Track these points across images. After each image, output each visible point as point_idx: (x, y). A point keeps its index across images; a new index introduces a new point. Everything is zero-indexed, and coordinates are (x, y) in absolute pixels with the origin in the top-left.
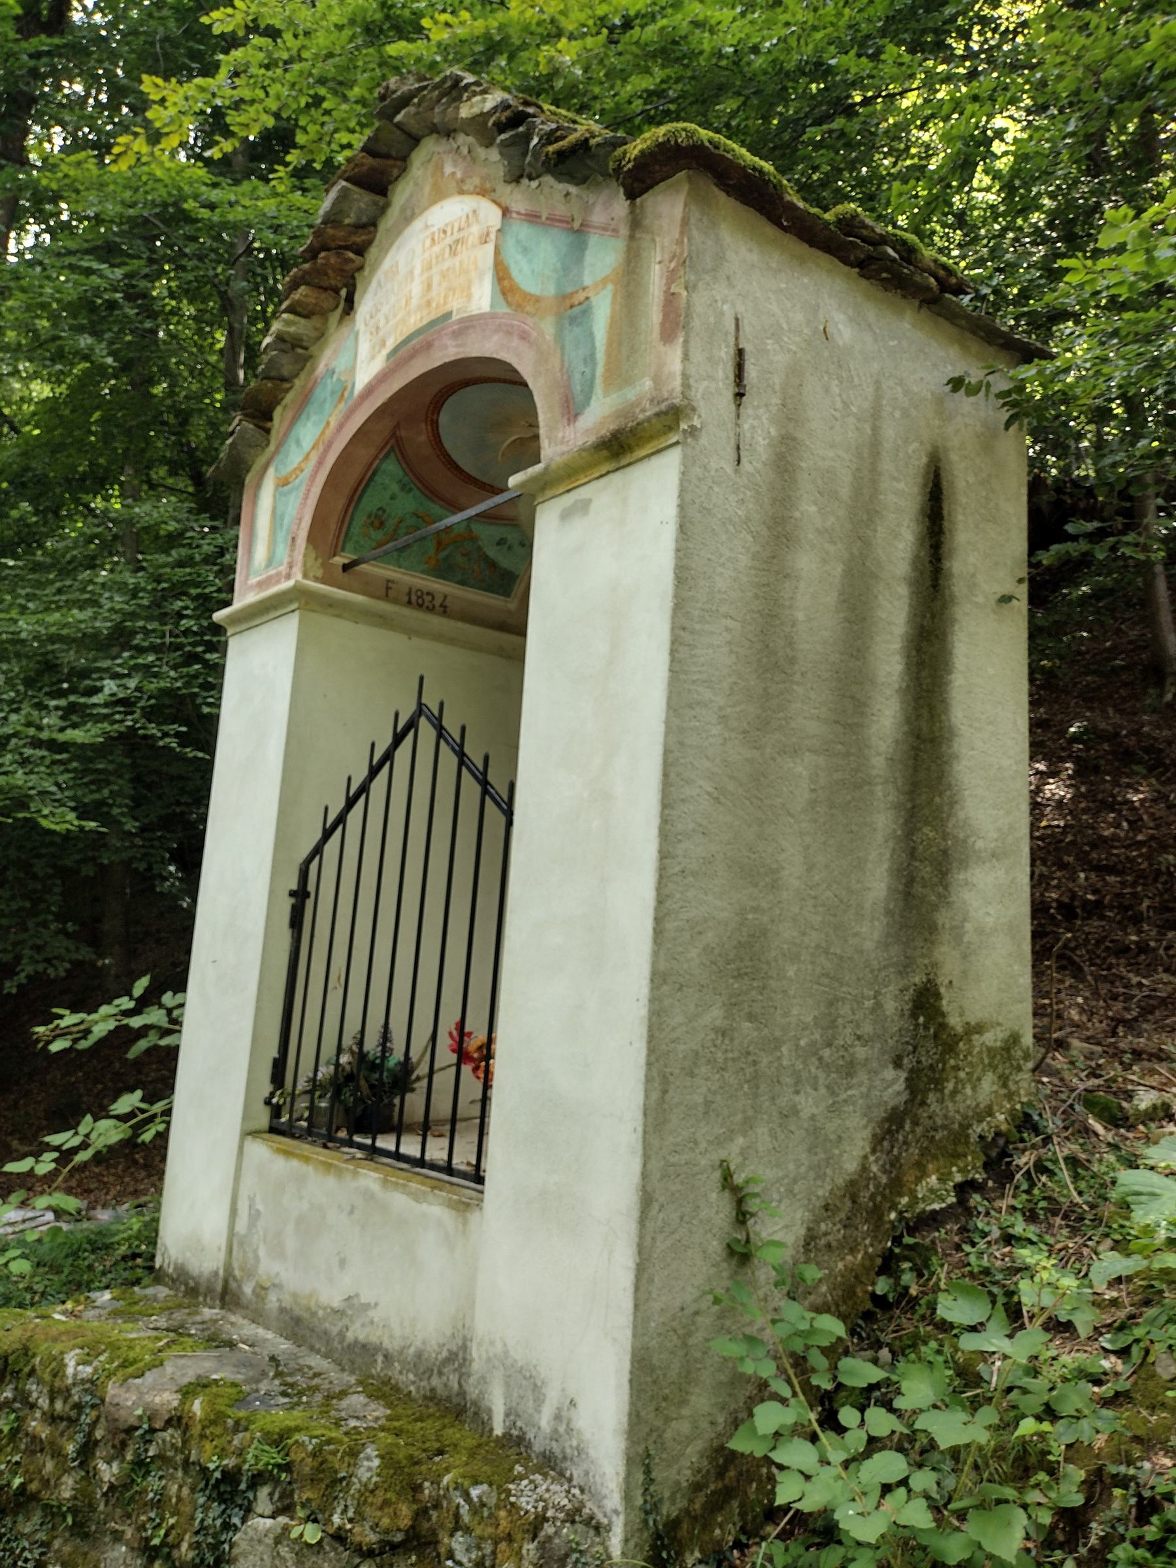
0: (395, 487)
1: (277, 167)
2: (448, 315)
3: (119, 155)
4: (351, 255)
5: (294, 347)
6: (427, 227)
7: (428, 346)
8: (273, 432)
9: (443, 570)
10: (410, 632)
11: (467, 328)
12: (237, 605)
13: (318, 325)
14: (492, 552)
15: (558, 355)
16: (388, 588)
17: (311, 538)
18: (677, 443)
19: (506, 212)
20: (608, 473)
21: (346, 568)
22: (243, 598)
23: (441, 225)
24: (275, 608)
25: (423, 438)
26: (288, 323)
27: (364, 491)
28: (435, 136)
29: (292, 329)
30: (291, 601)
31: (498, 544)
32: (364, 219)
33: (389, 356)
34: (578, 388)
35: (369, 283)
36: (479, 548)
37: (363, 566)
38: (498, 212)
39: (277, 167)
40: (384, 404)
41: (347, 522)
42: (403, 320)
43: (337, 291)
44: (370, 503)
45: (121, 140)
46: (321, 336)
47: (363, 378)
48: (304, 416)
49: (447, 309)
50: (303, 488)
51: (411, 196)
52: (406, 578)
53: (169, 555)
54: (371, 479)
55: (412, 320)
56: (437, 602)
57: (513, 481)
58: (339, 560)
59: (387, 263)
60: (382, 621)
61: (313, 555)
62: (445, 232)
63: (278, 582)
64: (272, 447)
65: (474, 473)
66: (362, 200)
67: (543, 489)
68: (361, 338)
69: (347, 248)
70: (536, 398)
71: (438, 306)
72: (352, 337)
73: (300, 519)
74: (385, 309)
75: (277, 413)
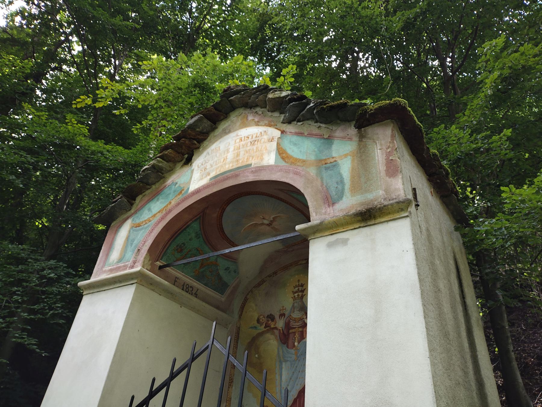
0: (193, 235)
1: (138, 124)
2: (251, 165)
3: (79, 102)
4: (195, 142)
5: (158, 171)
6: (237, 135)
7: (237, 176)
8: (135, 206)
9: (199, 278)
10: (182, 304)
11: (262, 170)
12: (94, 278)
13: (171, 166)
14: (222, 273)
15: (319, 180)
16: (175, 281)
17: (150, 250)
18: (407, 216)
19: (283, 132)
20: (360, 227)
21: (161, 268)
22: (99, 274)
23: (246, 135)
24: (120, 282)
25: (215, 215)
26: (158, 161)
27: (179, 234)
28: (243, 108)
29: (160, 164)
30: (132, 279)
31: (226, 269)
32: (205, 131)
33: (211, 179)
34: (334, 193)
35: (202, 153)
36: (218, 270)
37: (167, 268)
38: (280, 132)
39: (138, 124)
40: (206, 196)
41: (169, 248)
42: (222, 166)
43: (183, 155)
44: (180, 240)
45: (82, 97)
46: (171, 171)
47: (193, 187)
48: (156, 199)
49: (249, 162)
50: (150, 228)
51: (229, 125)
52: (184, 277)
53: (18, 267)
54: (185, 229)
55: (227, 166)
56: (194, 292)
57: (298, 227)
58: (158, 263)
59: (214, 146)
60: (170, 295)
61: (149, 259)
62: (248, 138)
63: (125, 269)
64: (132, 211)
65: (228, 236)
66: (207, 123)
67: (314, 233)
68: (195, 172)
69: (194, 139)
70: (306, 196)
71: (242, 162)
72: (189, 171)
73: (145, 242)
74: (211, 162)
75: (138, 199)
